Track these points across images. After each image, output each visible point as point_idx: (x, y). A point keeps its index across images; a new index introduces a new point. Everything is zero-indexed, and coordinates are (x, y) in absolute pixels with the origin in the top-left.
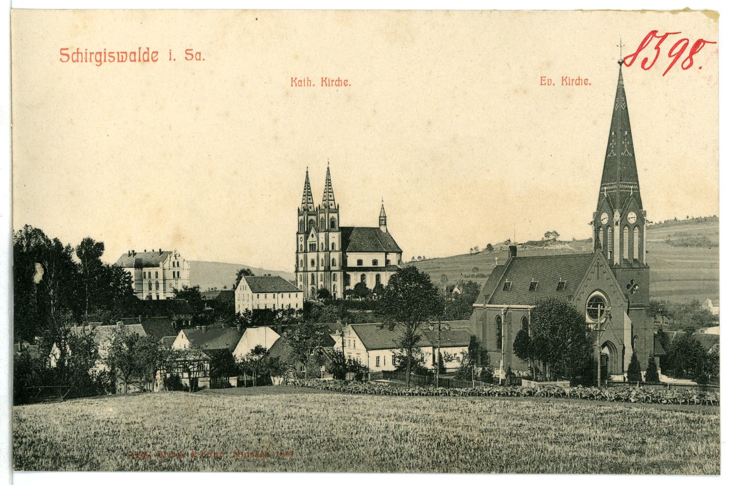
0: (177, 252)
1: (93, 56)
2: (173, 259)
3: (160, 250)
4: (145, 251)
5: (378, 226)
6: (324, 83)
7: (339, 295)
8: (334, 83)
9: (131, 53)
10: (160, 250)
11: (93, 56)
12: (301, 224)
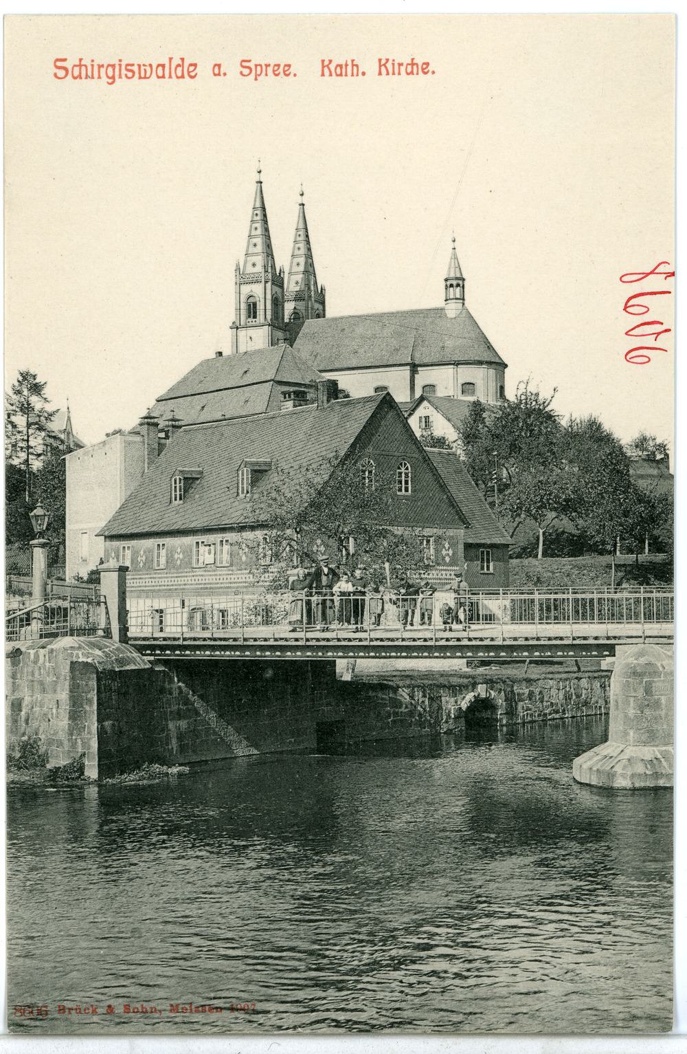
8: (403, 69)
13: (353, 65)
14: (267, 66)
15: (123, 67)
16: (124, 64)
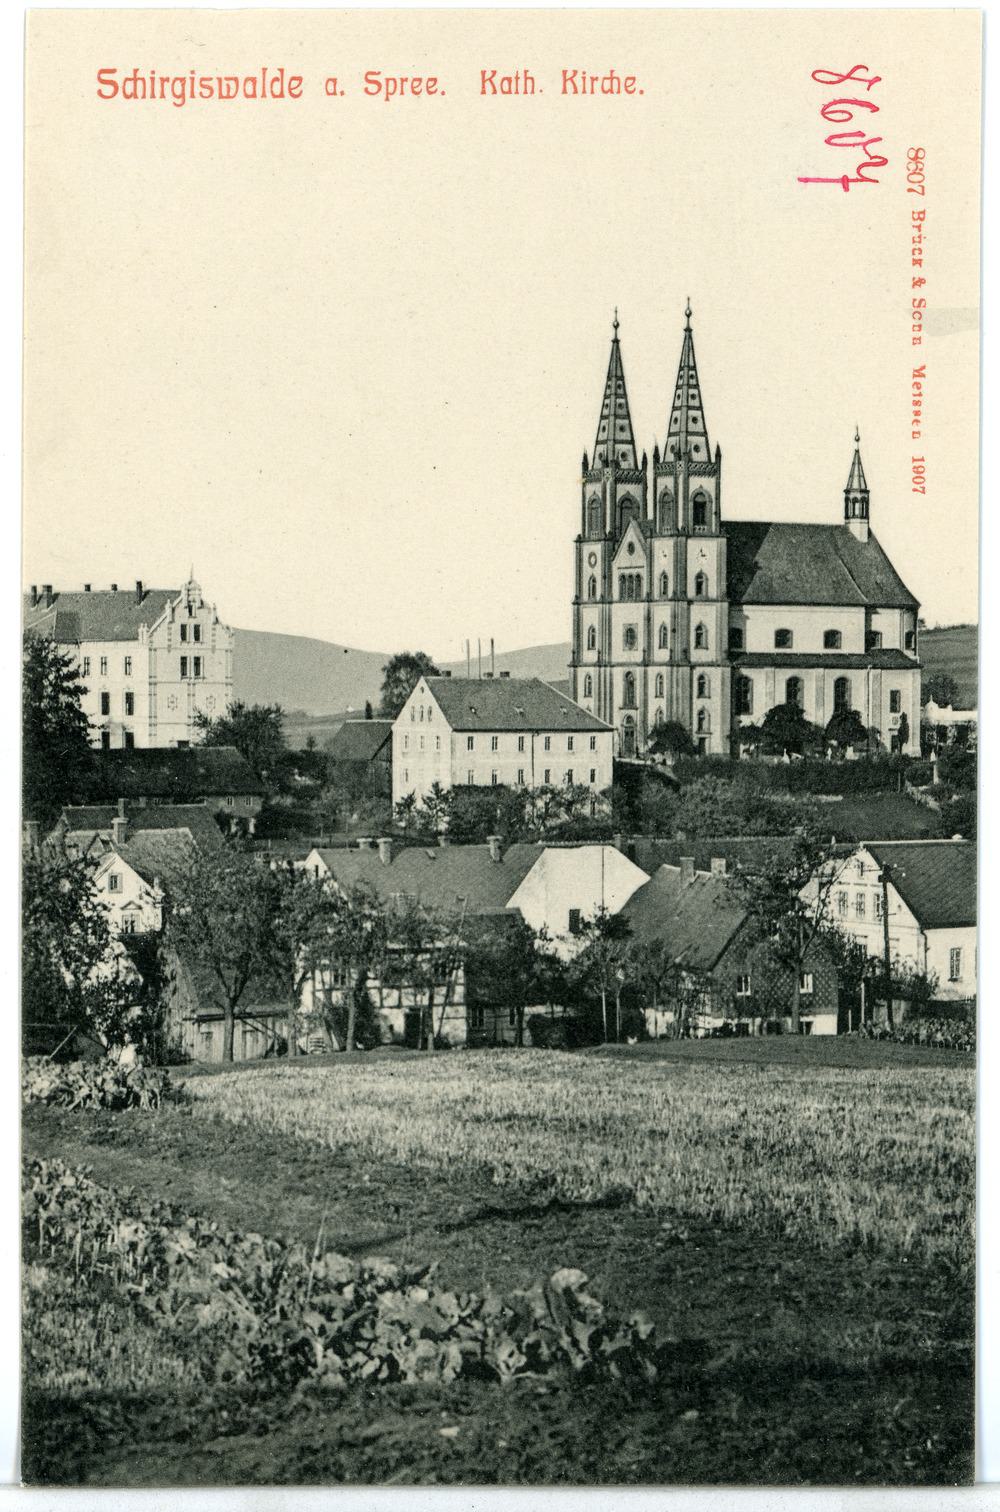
0: (194, 595)
1: (167, 86)
2: (182, 616)
3: (139, 584)
4: (88, 588)
5: (840, 520)
6: (569, 85)
7: (716, 745)
8: (597, 85)
9: (247, 80)
10: (139, 584)
11: (167, 86)
12: (591, 509)
13: (526, 78)
14: (404, 80)
15: (197, 84)
16: (197, 78)
